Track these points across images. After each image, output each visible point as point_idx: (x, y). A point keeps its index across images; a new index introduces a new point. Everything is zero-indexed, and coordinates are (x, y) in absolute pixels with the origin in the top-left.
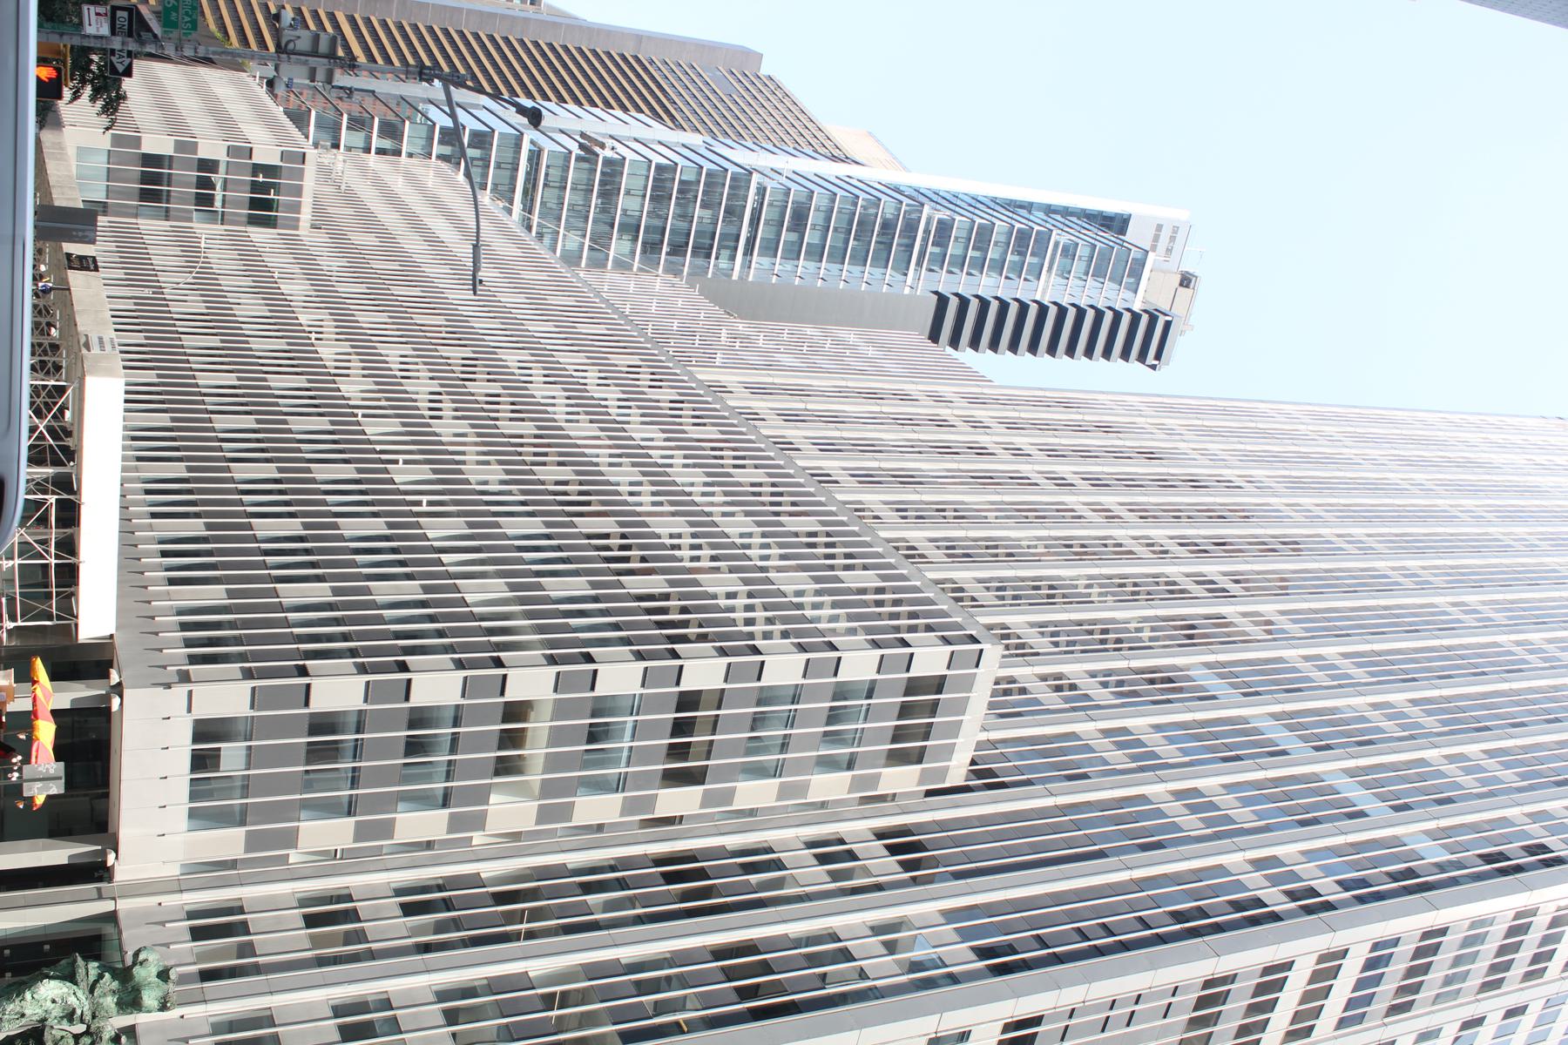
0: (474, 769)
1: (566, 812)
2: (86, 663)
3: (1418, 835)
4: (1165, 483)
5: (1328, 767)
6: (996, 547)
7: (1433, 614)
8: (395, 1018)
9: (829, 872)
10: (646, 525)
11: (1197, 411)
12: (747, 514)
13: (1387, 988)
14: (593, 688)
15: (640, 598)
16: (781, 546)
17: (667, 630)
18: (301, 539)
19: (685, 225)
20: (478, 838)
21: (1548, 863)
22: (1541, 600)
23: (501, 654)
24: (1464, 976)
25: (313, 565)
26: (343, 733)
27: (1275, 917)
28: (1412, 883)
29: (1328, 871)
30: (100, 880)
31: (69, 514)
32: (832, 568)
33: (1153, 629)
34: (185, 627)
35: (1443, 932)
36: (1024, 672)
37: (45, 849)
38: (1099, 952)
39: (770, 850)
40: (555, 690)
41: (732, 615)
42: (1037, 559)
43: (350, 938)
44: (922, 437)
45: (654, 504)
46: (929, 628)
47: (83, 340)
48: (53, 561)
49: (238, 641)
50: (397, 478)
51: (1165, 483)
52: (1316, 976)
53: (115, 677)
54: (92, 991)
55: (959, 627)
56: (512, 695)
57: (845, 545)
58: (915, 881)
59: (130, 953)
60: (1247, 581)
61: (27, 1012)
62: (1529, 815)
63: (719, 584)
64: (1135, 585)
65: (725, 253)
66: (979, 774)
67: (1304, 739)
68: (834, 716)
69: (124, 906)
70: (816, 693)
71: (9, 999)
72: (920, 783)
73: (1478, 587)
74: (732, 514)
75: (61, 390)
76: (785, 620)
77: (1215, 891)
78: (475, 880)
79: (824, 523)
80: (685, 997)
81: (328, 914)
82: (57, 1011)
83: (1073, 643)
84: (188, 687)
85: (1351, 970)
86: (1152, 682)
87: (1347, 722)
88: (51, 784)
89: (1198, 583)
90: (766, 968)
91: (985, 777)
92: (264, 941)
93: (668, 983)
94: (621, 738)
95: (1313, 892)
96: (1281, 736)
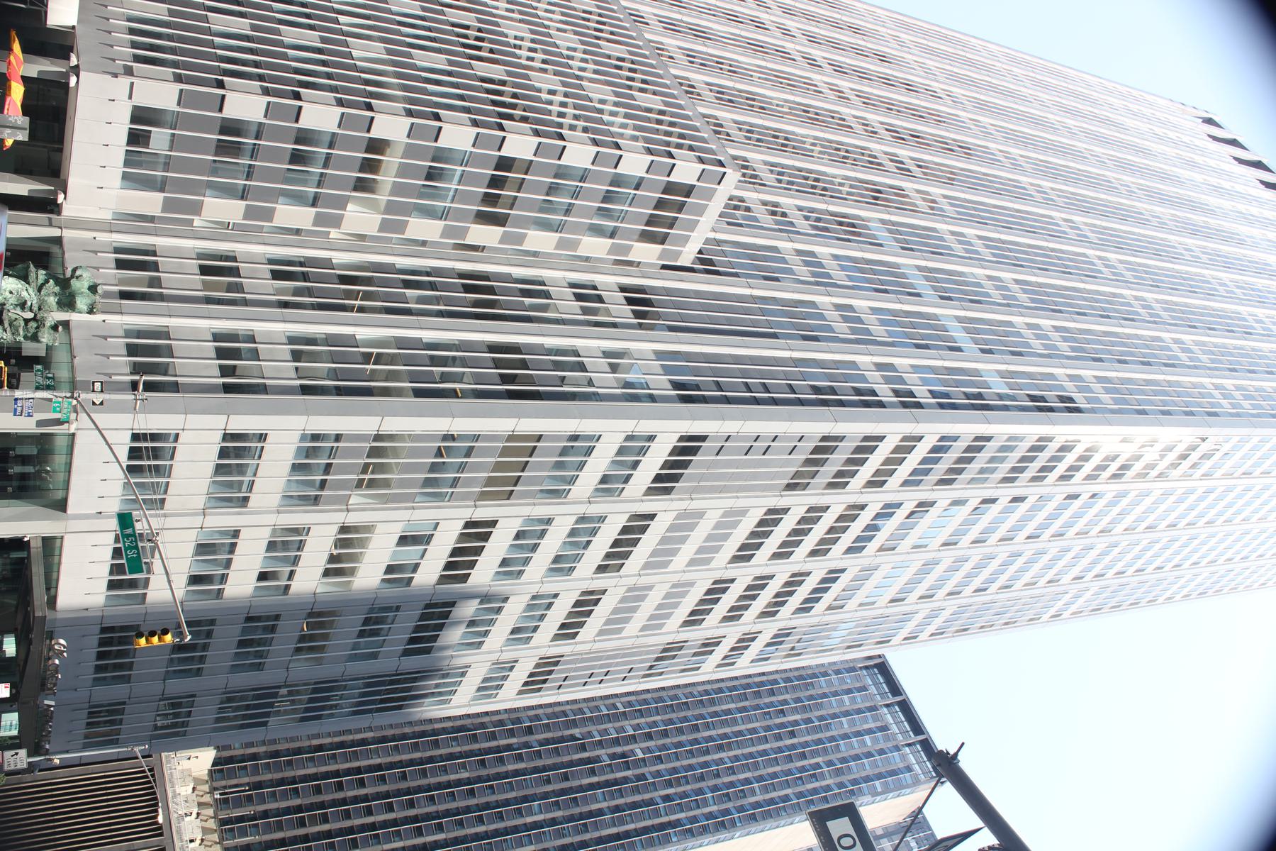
1: (401, 227)
3: (992, 372)
4: (887, 82)
5: (946, 312)
6: (754, 100)
7: (1048, 223)
8: (256, 349)
9: (582, 308)
10: (497, 25)
11: (926, 33)
12: (576, 33)
13: (941, 467)
14: (436, 140)
15: (483, 80)
16: (596, 63)
17: (499, 108)
20: (334, 234)
21: (1070, 410)
22: (1125, 232)
23: (373, 101)
24: (993, 470)
26: (245, 137)
27: (881, 405)
28: (979, 403)
29: (925, 382)
30: (51, 212)
32: (630, 88)
33: (851, 187)
34: (132, 31)
35: (988, 439)
36: (751, 196)
37: (10, 181)
38: (757, 401)
40: (408, 136)
41: (549, 107)
42: (781, 116)
44: (744, 34)
45: (508, 10)
46: (691, 148)
49: (173, 51)
51: (887, 82)
52: (897, 449)
54: (39, 290)
55: (712, 152)
56: (375, 133)
57: (644, 73)
58: (640, 326)
59: (70, 269)
60: (927, 168)
62: (1069, 376)
63: (545, 82)
64: (847, 151)
66: (702, 261)
67: (935, 289)
68: (608, 197)
69: (68, 234)
70: (598, 177)
72: (659, 259)
73: (1085, 211)
74: (565, 31)
76: (587, 119)
77: (847, 378)
78: (327, 263)
79: (631, 53)
80: (464, 373)
81: (218, 268)
83: (792, 183)
84: (131, 79)
85: (922, 450)
86: (841, 224)
87: (967, 284)
88: (18, 132)
89: (892, 161)
91: (706, 264)
93: (454, 361)
94: (450, 181)
95: (911, 394)
96: (920, 283)
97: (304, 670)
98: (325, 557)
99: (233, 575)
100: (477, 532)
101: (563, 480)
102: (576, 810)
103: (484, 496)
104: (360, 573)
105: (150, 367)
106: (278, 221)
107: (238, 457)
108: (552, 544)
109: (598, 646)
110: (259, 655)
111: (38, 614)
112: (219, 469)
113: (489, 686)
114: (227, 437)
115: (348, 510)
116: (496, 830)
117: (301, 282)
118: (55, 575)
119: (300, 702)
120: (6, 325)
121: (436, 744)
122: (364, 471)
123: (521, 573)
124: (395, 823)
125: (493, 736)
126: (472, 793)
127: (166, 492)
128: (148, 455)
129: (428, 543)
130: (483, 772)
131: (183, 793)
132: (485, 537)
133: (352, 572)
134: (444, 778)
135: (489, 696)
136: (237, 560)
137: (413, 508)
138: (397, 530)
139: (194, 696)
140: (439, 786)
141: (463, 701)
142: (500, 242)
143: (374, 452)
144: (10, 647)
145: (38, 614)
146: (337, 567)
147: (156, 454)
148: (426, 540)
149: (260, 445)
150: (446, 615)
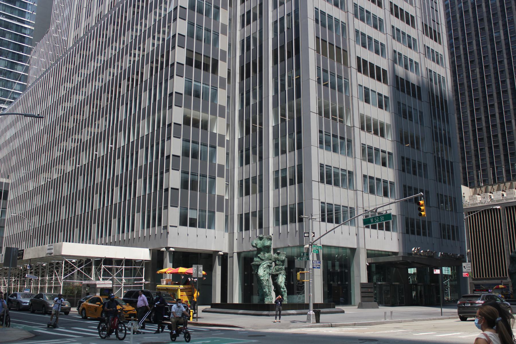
0: (205, 137)
1: (222, 108)
2: (158, 258)
9: (253, 21)
17: (164, 66)
18: (121, 188)
19: (12, 45)
20: (227, 138)
25: (130, 184)
30: (227, 257)
31: (108, 261)
34: (148, 227)
37: (216, 273)
39: (243, 41)
40: (181, 107)
43: (254, 182)
47: (49, 255)
48: (124, 267)
49: (154, 210)
50: (102, 154)
53: (164, 249)
54: (263, 260)
56: (181, 122)
61: (267, 278)
63: (149, 46)
65: (23, 31)
69: (236, 250)
71: (262, 284)
75: (66, 262)
78: (241, 140)
80: (288, 76)
81: (246, 188)
82: (268, 270)
90: (282, 47)
92: (252, 208)
93: (283, 80)
97: (427, 146)
98: (375, 137)
99: (384, 177)
100: (364, 66)
101: (411, 64)
102: (499, 14)
103: (346, 64)
104: (383, 120)
105: (293, 214)
106: (224, 163)
107: (330, 177)
108: (368, 30)
109: (418, 5)
110: (420, 165)
111: (401, 259)
112: (336, 184)
113: (437, 59)
114: (322, 181)
115: (354, 126)
116: (507, 54)
117: (251, 150)
118: (383, 253)
119: (442, 147)
120: (278, 273)
121: (462, 85)
122: (336, 120)
123: (382, 44)
124: (500, 103)
125: (459, 57)
126: (487, 67)
127: (347, 207)
128: (332, 215)
129: (368, 89)
130: (477, 61)
131: (480, 199)
132: (365, 62)
133: (382, 124)
134: (479, 80)
135: (441, 58)
136: (377, 175)
137: (352, 96)
138: (362, 104)
139: (438, 194)
140: (483, 82)
141: (444, 71)
142: (226, 62)
143: (327, 115)
144: (412, 271)
145: (401, 259)
146: (379, 130)
147: (330, 211)
148: (367, 90)
149: (325, 167)
150: (402, 79)
